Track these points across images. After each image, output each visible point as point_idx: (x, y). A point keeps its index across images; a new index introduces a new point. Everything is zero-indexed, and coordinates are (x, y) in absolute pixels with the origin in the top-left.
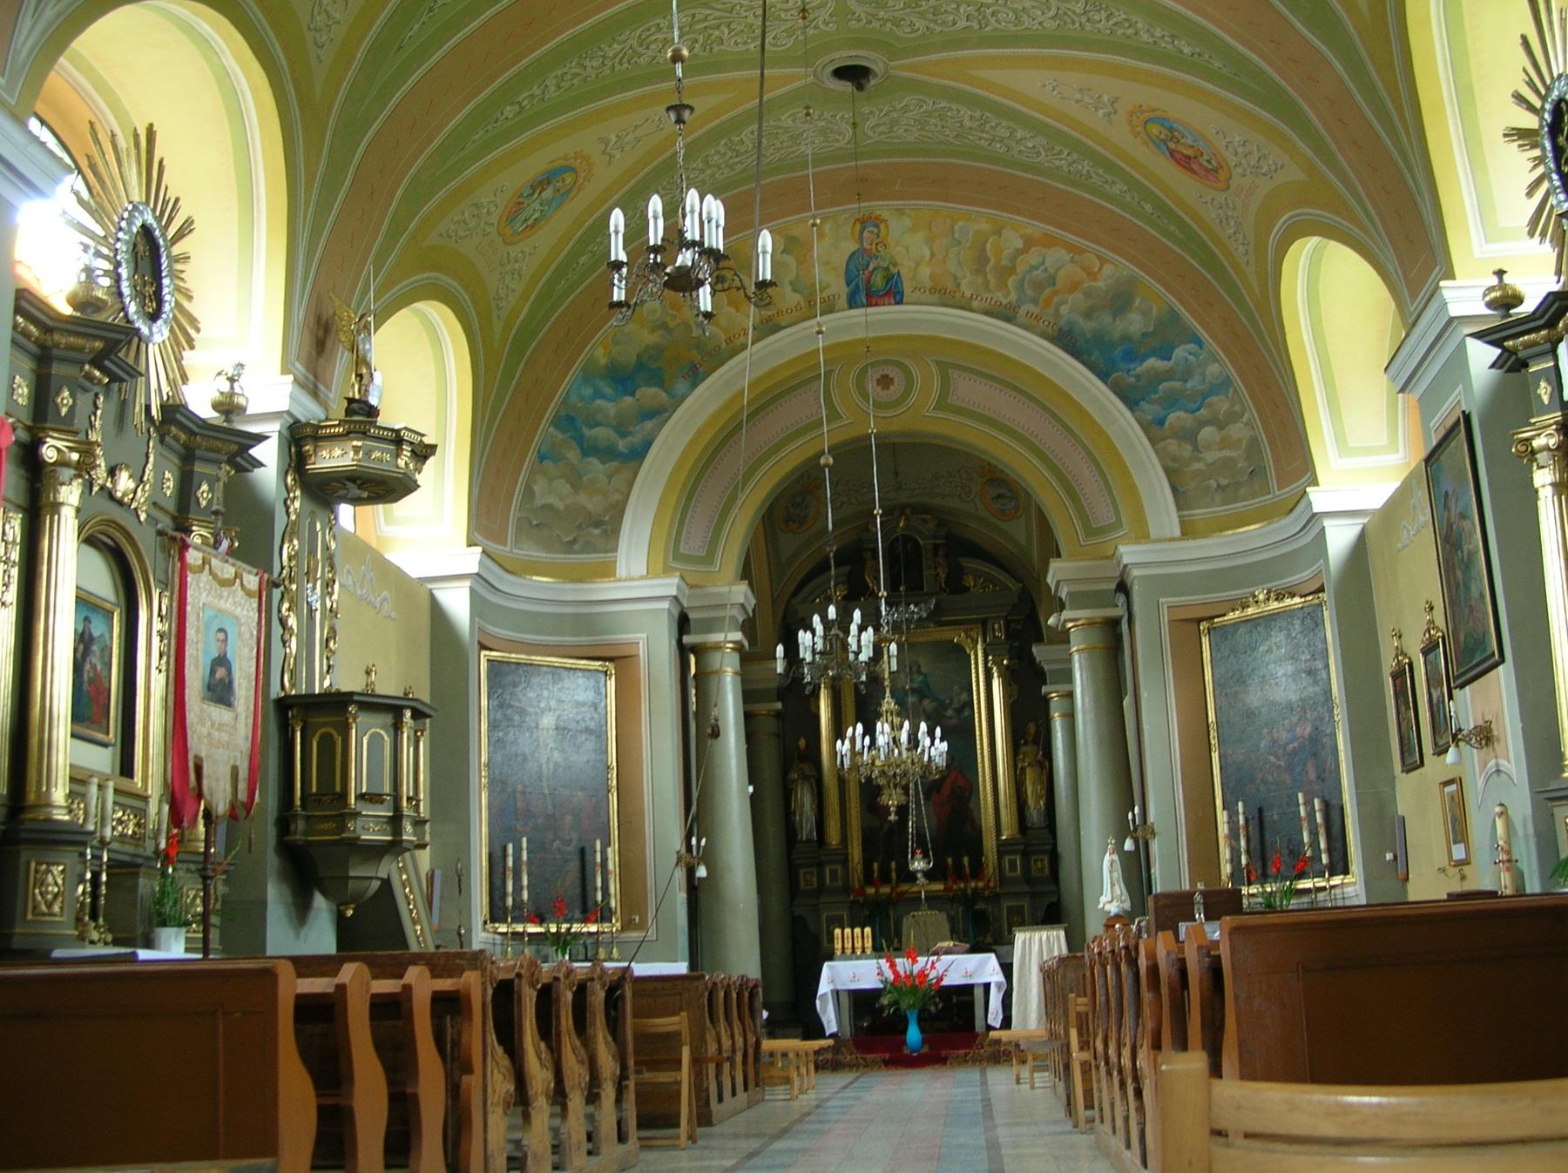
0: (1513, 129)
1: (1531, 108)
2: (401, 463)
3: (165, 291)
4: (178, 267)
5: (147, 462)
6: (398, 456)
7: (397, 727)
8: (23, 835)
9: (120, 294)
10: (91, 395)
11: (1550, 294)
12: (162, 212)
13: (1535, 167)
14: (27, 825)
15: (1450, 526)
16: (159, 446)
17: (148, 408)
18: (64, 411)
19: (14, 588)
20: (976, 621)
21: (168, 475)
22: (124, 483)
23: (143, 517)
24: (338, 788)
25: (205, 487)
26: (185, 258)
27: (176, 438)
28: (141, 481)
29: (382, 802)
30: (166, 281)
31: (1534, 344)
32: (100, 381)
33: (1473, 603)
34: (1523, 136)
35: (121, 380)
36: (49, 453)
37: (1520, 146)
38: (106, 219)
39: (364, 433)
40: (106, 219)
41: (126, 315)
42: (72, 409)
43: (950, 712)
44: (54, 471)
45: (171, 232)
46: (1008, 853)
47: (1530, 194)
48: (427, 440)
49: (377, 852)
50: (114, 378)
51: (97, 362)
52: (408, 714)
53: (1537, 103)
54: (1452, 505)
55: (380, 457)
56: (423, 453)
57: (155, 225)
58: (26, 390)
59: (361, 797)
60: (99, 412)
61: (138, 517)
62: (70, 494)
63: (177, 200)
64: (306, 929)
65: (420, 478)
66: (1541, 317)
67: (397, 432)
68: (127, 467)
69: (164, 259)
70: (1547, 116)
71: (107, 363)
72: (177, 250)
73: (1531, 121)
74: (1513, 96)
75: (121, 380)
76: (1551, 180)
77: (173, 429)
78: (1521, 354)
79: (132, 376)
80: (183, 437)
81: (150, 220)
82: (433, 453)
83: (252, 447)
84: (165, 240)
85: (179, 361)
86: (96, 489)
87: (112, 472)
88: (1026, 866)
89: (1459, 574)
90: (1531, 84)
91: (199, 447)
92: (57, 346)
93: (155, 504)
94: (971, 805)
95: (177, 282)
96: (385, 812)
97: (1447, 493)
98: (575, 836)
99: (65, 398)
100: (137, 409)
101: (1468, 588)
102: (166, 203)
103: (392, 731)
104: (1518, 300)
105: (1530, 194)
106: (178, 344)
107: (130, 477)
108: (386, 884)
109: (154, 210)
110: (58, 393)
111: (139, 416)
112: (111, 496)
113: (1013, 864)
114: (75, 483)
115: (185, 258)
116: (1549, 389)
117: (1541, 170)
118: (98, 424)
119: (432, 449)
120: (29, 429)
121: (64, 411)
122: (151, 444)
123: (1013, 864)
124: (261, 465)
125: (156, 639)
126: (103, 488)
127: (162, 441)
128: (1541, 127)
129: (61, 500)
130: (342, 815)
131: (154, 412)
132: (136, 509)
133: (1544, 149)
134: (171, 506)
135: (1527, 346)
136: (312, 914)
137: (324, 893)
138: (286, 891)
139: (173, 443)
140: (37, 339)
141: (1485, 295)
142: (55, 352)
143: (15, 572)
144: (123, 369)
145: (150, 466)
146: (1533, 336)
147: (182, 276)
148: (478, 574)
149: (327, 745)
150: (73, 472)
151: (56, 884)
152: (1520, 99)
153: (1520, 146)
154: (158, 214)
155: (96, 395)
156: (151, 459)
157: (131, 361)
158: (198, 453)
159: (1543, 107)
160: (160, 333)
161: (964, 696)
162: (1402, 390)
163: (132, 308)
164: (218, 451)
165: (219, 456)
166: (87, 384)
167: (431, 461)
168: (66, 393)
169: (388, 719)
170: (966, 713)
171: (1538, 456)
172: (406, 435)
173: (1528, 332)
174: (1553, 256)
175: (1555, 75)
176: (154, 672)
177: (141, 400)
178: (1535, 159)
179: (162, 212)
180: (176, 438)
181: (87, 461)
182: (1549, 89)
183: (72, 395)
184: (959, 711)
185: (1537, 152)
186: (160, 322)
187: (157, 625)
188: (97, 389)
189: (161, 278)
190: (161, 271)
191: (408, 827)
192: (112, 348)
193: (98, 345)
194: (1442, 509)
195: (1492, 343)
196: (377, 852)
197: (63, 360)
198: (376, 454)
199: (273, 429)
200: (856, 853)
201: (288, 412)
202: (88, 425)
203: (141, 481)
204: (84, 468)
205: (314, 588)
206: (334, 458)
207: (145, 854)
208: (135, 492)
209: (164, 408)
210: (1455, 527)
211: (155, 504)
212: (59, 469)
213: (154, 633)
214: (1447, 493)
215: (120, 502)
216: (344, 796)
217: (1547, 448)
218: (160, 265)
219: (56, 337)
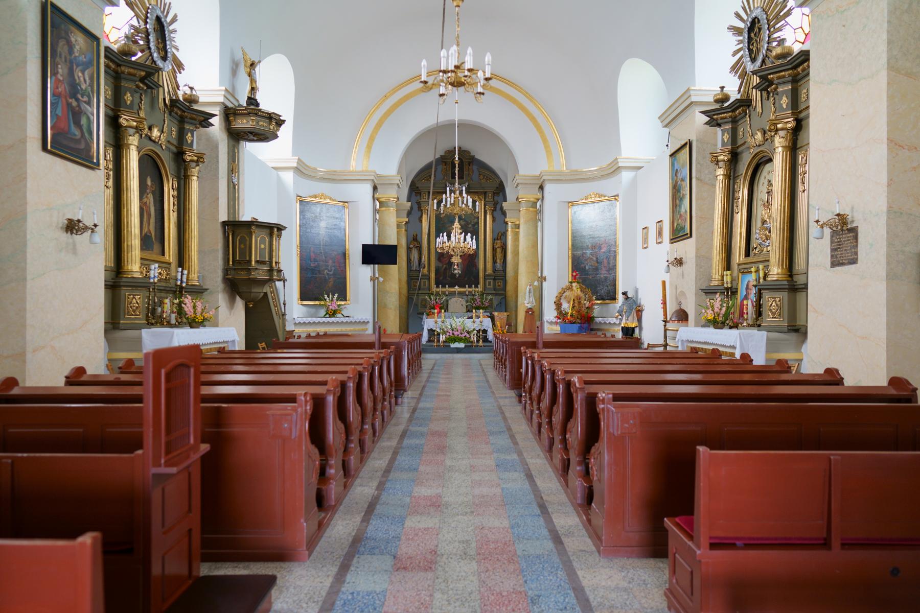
0: (732, 26)
1: (741, 19)
2: (271, 127)
3: (168, 47)
4: (172, 35)
5: (164, 123)
6: (270, 124)
7: (271, 235)
8: (122, 284)
9: (149, 48)
10: (139, 94)
11: (736, 100)
12: (164, 9)
13: (738, 44)
14: (124, 280)
15: (676, 182)
16: (169, 116)
17: (164, 100)
18: (129, 102)
19: (111, 180)
20: (481, 193)
21: (173, 129)
22: (156, 133)
23: (164, 147)
24: (248, 259)
25: (189, 135)
26: (175, 31)
27: (176, 113)
28: (162, 132)
29: (265, 264)
30: (168, 43)
31: (725, 118)
32: (143, 89)
33: (682, 213)
34: (737, 31)
35: (152, 88)
36: (123, 121)
37: (733, 34)
38: (136, 8)
39: (256, 114)
40: (136, 8)
41: (152, 58)
42: (132, 102)
43: (470, 226)
44: (126, 130)
45: (169, 19)
46: (488, 279)
47: (734, 55)
48: (281, 118)
49: (263, 282)
50: (149, 87)
51: (142, 80)
52: (276, 230)
53: (745, 17)
54: (679, 174)
55: (263, 124)
56: (280, 123)
57: (162, 16)
58: (110, 92)
59: (257, 262)
60: (143, 102)
61: (162, 147)
62: (133, 140)
63: (170, 4)
64: (233, 311)
65: (279, 133)
66: (731, 108)
67: (270, 114)
68: (157, 126)
69: (166, 32)
70: (748, 24)
71: (146, 81)
72: (171, 28)
73: (741, 25)
74: (735, 13)
75: (152, 88)
76: (744, 51)
77: (175, 109)
78: (719, 122)
79: (157, 87)
80: (179, 113)
81: (160, 14)
82: (283, 123)
83: (210, 119)
84: (166, 23)
85: (175, 78)
86: (143, 136)
87: (150, 128)
88: (494, 285)
89: (678, 201)
90: (744, 8)
91: (186, 117)
92: (123, 73)
93: (169, 142)
94: (476, 260)
95: (173, 43)
96: (266, 267)
97: (677, 170)
98: (333, 268)
99: (128, 97)
100: (160, 100)
101: (680, 207)
102: (165, 5)
103: (269, 236)
104: (727, 98)
105: (734, 55)
106: (175, 71)
107: (158, 130)
108: (266, 294)
109: (160, 8)
110: (125, 94)
111: (161, 104)
112: (150, 139)
113: (490, 283)
114: (136, 136)
115: (175, 31)
116: (728, 136)
117: (741, 45)
118: (142, 107)
119: (284, 121)
120: (112, 110)
121: (129, 102)
122: (166, 116)
123: (490, 283)
124: (212, 125)
125: (171, 198)
126: (146, 135)
127: (170, 114)
128: (745, 27)
129: (130, 143)
130: (249, 269)
131: (167, 102)
132: (161, 144)
133: (744, 37)
134: (175, 142)
135: (722, 118)
136: (236, 305)
137: (241, 297)
138: (226, 296)
139: (175, 115)
140: (114, 69)
141: (715, 96)
142: (122, 75)
143: (111, 173)
144: (153, 84)
145: (165, 125)
146: (725, 115)
147: (174, 39)
148: (296, 167)
149: (242, 241)
150: (134, 130)
151: (137, 303)
152: (737, 15)
153: (733, 34)
154: (162, 9)
155: (141, 95)
156: (166, 122)
157: (156, 80)
158: (186, 120)
159: (748, 19)
160: (168, 67)
161: (476, 220)
162: (666, 126)
163: (155, 55)
164: (195, 119)
165: (196, 122)
166: (137, 89)
167: (283, 126)
168: (129, 95)
169: (268, 231)
170: (476, 226)
171: (719, 163)
172: (274, 116)
173: (724, 113)
174: (739, 82)
175: (756, 6)
176: (171, 212)
177: (161, 97)
178: (739, 41)
179: (164, 9)
180: (176, 113)
181: (141, 126)
182: (751, 14)
183: (132, 96)
184: (474, 225)
185: (741, 38)
186: (167, 62)
187: (171, 193)
188: (141, 92)
189: (166, 41)
190: (165, 38)
191: (275, 273)
192: (149, 75)
193: (143, 74)
194: (674, 175)
195: (707, 116)
196: (263, 282)
197: (126, 79)
198: (261, 123)
199: (216, 111)
200: (433, 276)
201: (223, 103)
202: (138, 107)
203: (162, 132)
204: (138, 129)
205: (235, 176)
206: (242, 123)
207: (170, 286)
208: (160, 137)
209: (171, 100)
210: (678, 183)
211: (169, 142)
212: (128, 129)
213: (171, 196)
214: (677, 170)
215: (154, 141)
216: (250, 261)
217: (723, 161)
218: (165, 35)
219: (123, 68)
